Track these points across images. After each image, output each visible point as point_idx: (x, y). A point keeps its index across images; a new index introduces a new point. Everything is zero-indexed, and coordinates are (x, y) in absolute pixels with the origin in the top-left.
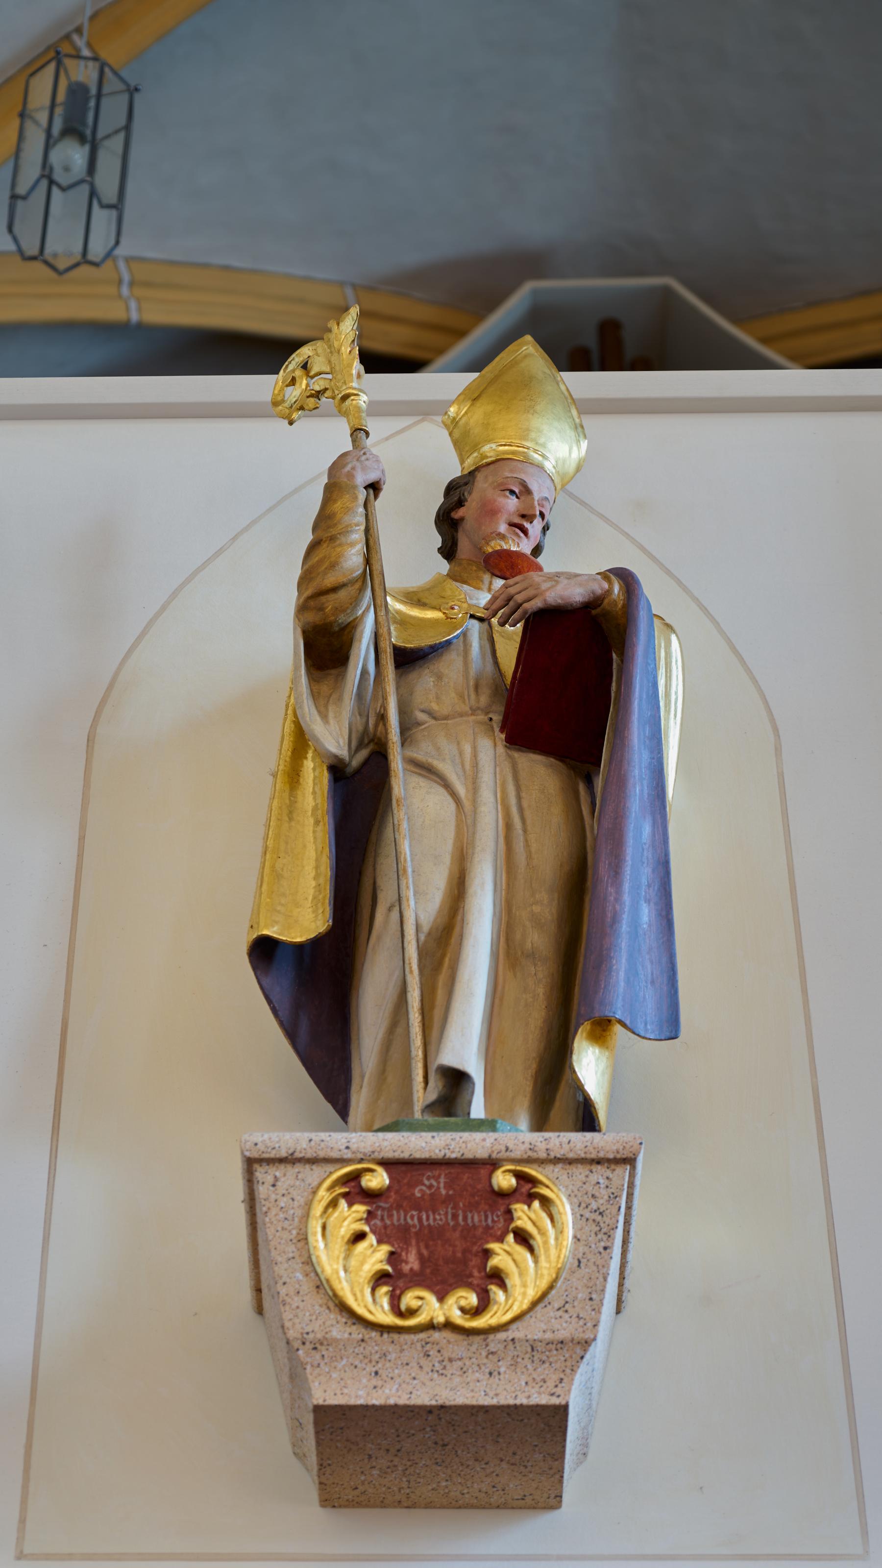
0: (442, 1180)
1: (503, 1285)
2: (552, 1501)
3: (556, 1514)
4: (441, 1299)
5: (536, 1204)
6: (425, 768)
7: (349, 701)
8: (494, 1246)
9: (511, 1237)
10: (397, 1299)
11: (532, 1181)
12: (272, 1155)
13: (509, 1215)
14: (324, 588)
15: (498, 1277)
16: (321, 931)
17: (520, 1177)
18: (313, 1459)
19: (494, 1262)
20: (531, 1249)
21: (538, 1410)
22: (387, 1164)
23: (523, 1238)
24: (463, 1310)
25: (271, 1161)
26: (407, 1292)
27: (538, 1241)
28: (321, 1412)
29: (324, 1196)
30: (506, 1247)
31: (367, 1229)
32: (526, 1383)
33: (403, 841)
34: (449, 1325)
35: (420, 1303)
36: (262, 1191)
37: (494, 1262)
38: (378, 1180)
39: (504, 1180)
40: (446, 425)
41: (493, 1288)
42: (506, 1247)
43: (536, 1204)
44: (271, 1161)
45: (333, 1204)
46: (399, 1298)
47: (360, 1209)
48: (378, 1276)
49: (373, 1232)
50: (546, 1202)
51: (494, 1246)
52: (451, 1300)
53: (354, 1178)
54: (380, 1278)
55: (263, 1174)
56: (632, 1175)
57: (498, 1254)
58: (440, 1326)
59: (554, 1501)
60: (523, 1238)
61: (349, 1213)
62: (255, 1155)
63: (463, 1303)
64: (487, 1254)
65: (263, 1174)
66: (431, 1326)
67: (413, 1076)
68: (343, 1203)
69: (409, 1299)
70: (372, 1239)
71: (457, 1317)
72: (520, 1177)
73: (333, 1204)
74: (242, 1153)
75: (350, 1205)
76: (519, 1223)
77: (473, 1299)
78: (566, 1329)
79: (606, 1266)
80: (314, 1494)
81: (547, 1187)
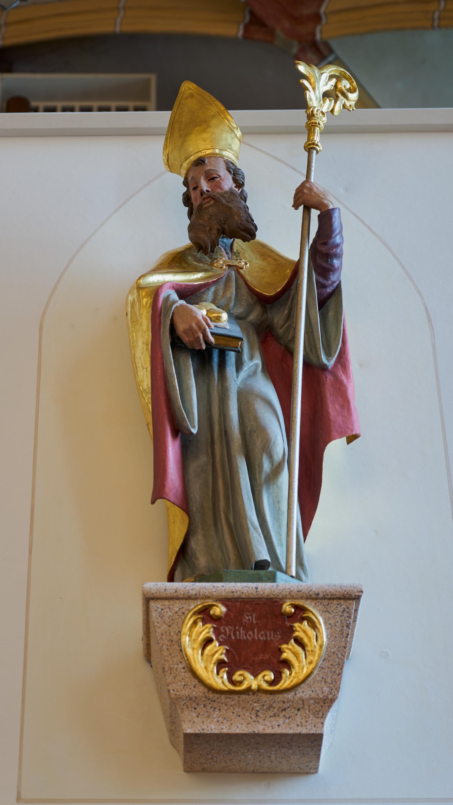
0: (254, 615)
1: (289, 669)
2: (312, 771)
4: (255, 676)
5: (305, 623)
6: (183, 599)
7: (276, 423)
9: (292, 641)
13: (292, 630)
14: (259, 415)
15: (287, 664)
16: (215, 445)
17: (296, 607)
18: (182, 746)
19: (284, 655)
21: (308, 736)
22: (225, 601)
24: (267, 682)
30: (290, 646)
33: (196, 561)
34: (260, 690)
36: (154, 615)
37: (284, 655)
39: (288, 608)
43: (305, 623)
45: (195, 623)
48: (220, 662)
49: (218, 639)
52: (260, 677)
54: (220, 664)
55: (152, 604)
62: (150, 595)
63: (266, 678)
64: (281, 652)
65: (152, 604)
66: (249, 690)
68: (200, 624)
69: (236, 677)
70: (216, 643)
71: (265, 686)
72: (296, 607)
73: (195, 623)
74: (143, 590)
76: (296, 634)
77: (271, 676)
80: (182, 768)
81: (312, 612)
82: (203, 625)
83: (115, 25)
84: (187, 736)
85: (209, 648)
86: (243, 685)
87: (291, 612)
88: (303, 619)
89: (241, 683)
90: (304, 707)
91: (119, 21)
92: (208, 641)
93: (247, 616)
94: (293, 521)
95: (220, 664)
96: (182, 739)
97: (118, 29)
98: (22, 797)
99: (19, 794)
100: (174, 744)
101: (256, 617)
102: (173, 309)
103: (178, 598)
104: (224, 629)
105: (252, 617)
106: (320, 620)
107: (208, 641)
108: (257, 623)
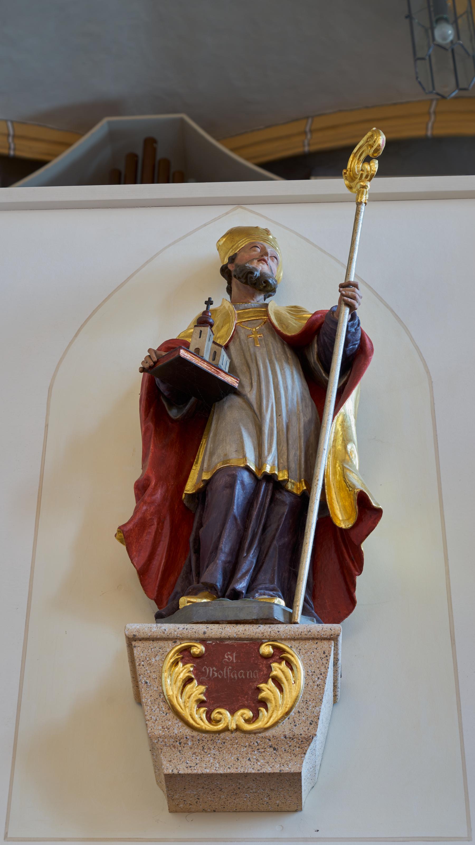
0: (234, 655)
3: (296, 816)
4: (233, 713)
5: (284, 663)
8: (262, 686)
10: (204, 469)
11: (283, 651)
12: (142, 636)
13: (270, 669)
15: (264, 703)
19: (262, 695)
20: (281, 690)
22: (202, 641)
23: (278, 683)
25: (141, 639)
26: (216, 709)
27: (286, 685)
28: (170, 778)
29: (170, 659)
31: (193, 676)
32: (291, 628)
35: (221, 716)
37: (262, 695)
38: (199, 649)
39: (266, 649)
40: (232, 259)
41: (263, 709)
42: (268, 686)
43: (284, 663)
44: (141, 639)
45: (175, 663)
46: (211, 715)
47: (189, 667)
50: (289, 664)
51: (262, 686)
53: (187, 650)
54: (201, 703)
56: (336, 645)
57: (263, 690)
58: (232, 730)
59: (298, 808)
60: (278, 683)
61: (183, 668)
64: (259, 690)
67: (217, 637)
68: (180, 664)
69: (215, 715)
70: (195, 681)
72: (274, 647)
73: (175, 663)
75: (184, 664)
76: (274, 673)
78: (300, 730)
79: (327, 663)
81: (288, 653)
82: (183, 666)
83: (427, 129)
84: (166, 775)
85: (189, 687)
86: (220, 724)
87: (202, 650)
88: (282, 659)
89: (218, 722)
90: (242, 747)
91: (430, 125)
92: (188, 681)
93: (228, 655)
94: (305, 564)
95: (201, 703)
96: (163, 776)
97: (429, 133)
98: (9, 836)
99: (6, 834)
100: (159, 783)
101: (236, 656)
102: (168, 353)
103: (308, 639)
104: (205, 669)
105: (232, 656)
106: (298, 661)
107: (188, 681)
108: (237, 662)
